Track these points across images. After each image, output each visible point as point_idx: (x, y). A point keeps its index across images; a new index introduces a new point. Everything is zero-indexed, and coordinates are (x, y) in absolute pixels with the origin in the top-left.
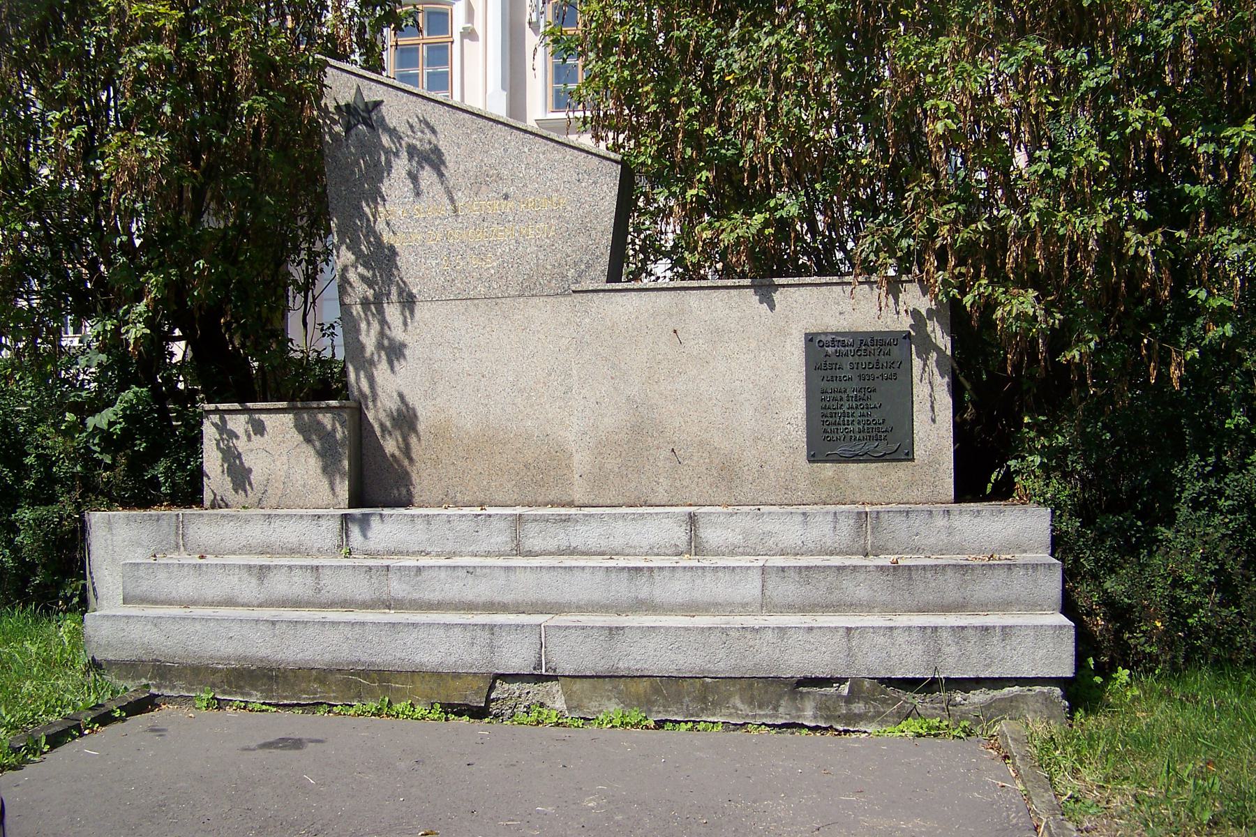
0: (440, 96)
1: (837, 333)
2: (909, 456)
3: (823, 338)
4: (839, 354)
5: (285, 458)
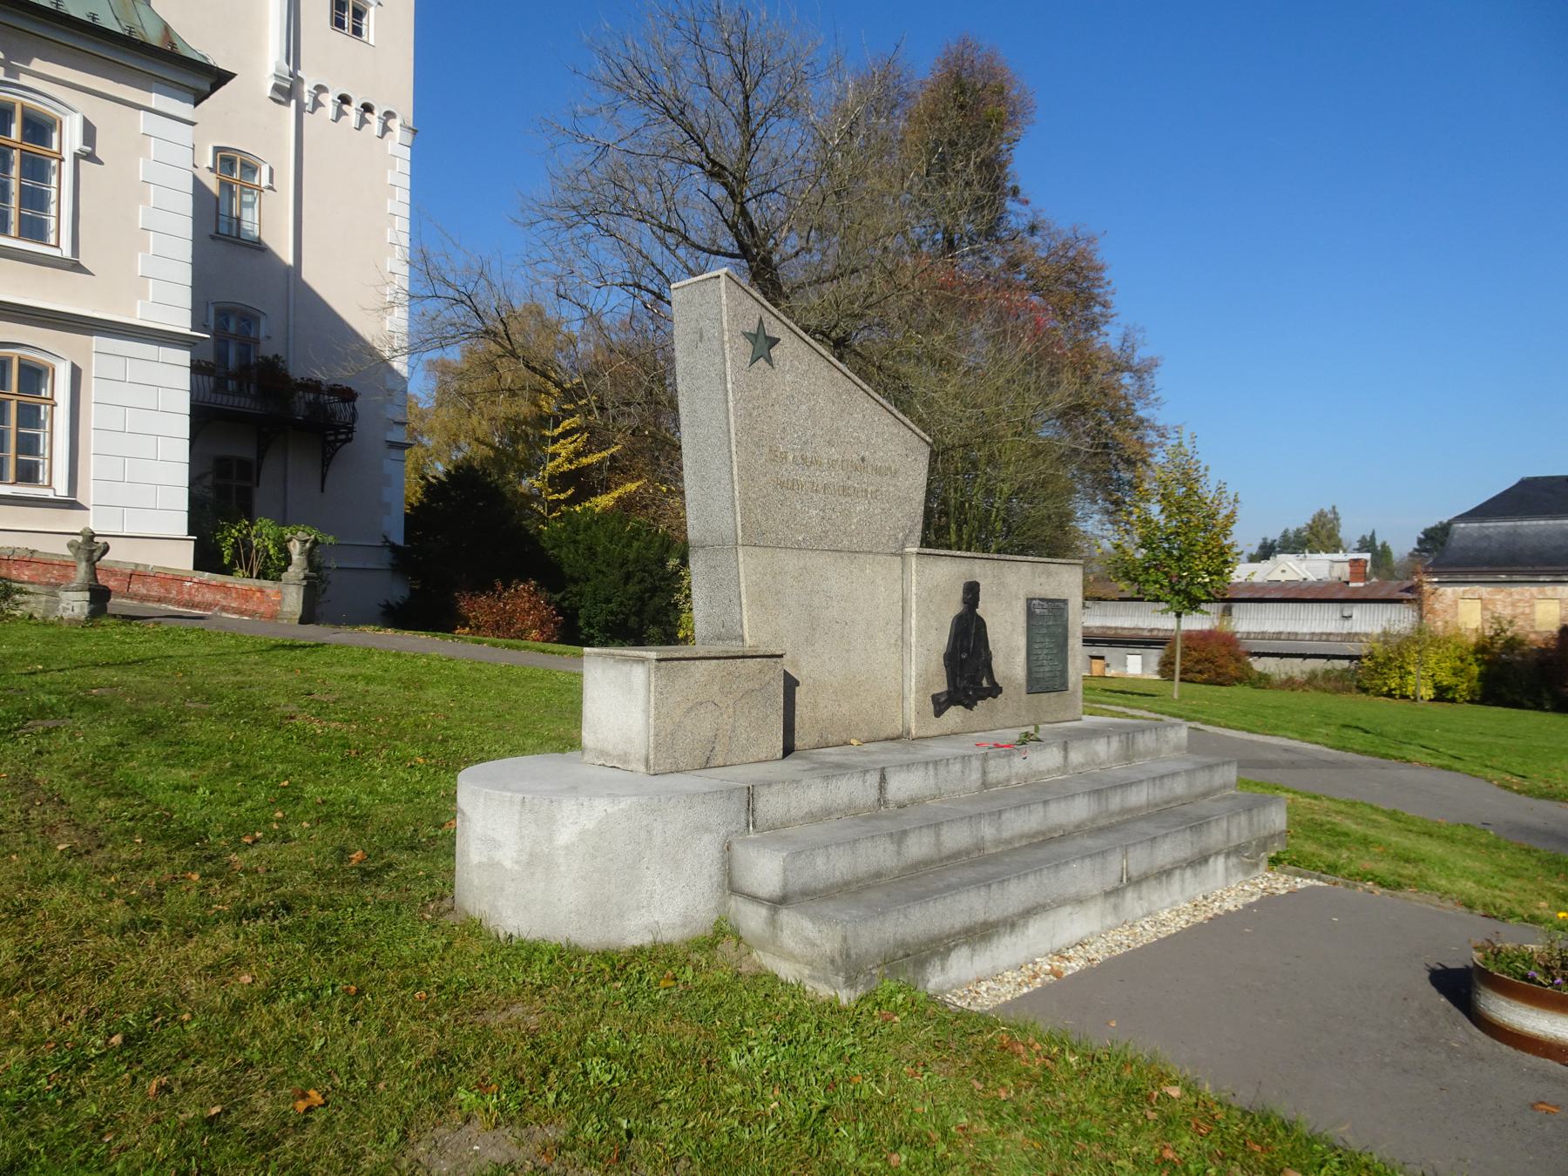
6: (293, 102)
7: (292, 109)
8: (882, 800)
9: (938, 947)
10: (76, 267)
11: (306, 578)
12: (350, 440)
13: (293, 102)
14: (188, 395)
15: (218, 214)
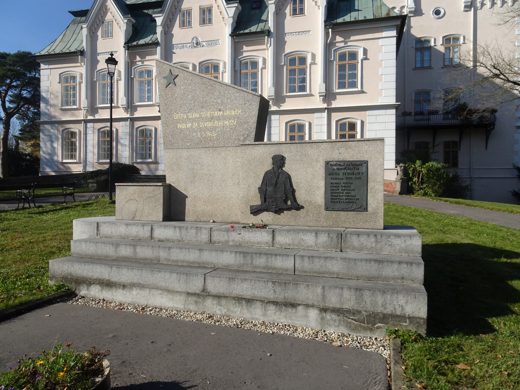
0: (293, 142)
1: (338, 161)
2: (366, 209)
3: (332, 163)
4: (338, 169)
5: (142, 203)
6: (473, 9)
7: (472, 13)
8: (152, 237)
9: (89, 282)
10: (362, 92)
11: (401, 179)
12: (494, 128)
13: (473, 9)
14: (395, 123)
15: (444, 59)
